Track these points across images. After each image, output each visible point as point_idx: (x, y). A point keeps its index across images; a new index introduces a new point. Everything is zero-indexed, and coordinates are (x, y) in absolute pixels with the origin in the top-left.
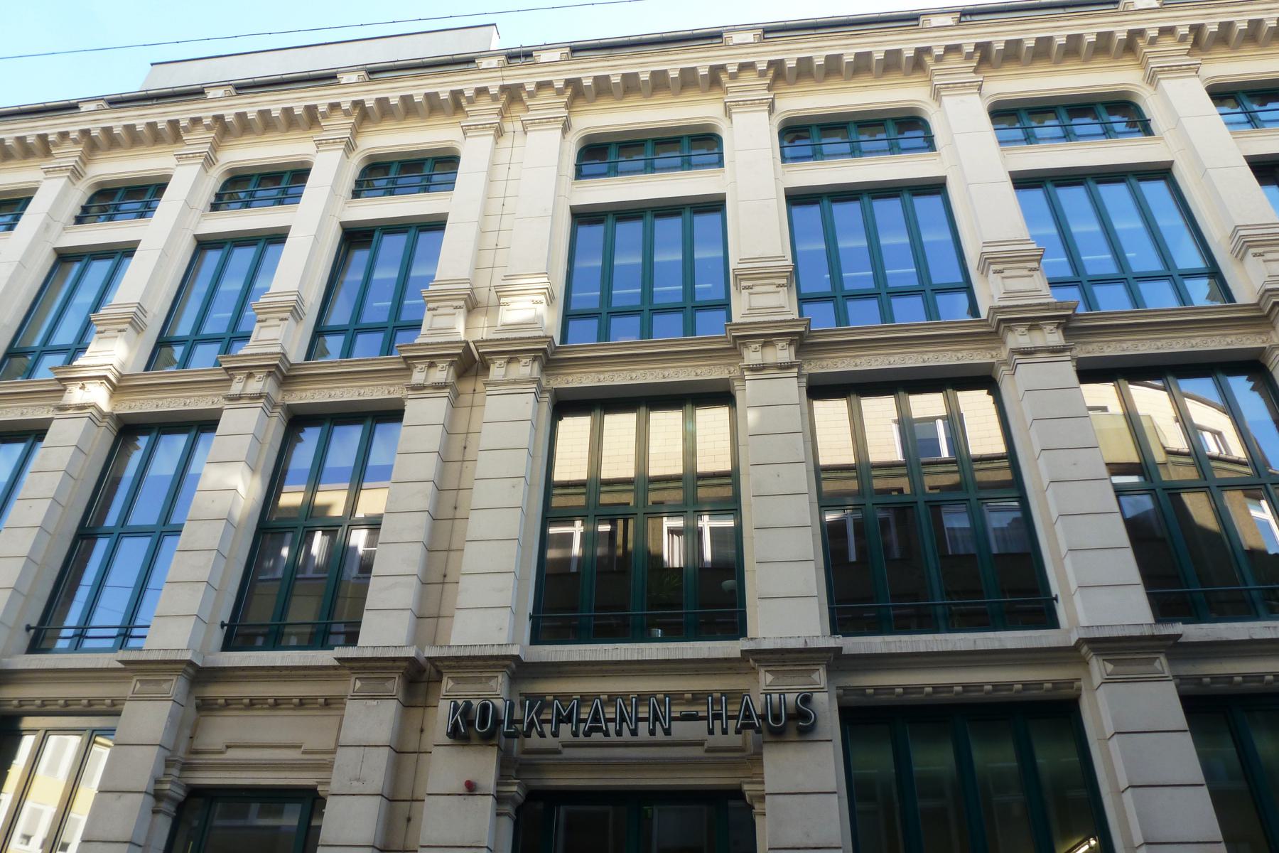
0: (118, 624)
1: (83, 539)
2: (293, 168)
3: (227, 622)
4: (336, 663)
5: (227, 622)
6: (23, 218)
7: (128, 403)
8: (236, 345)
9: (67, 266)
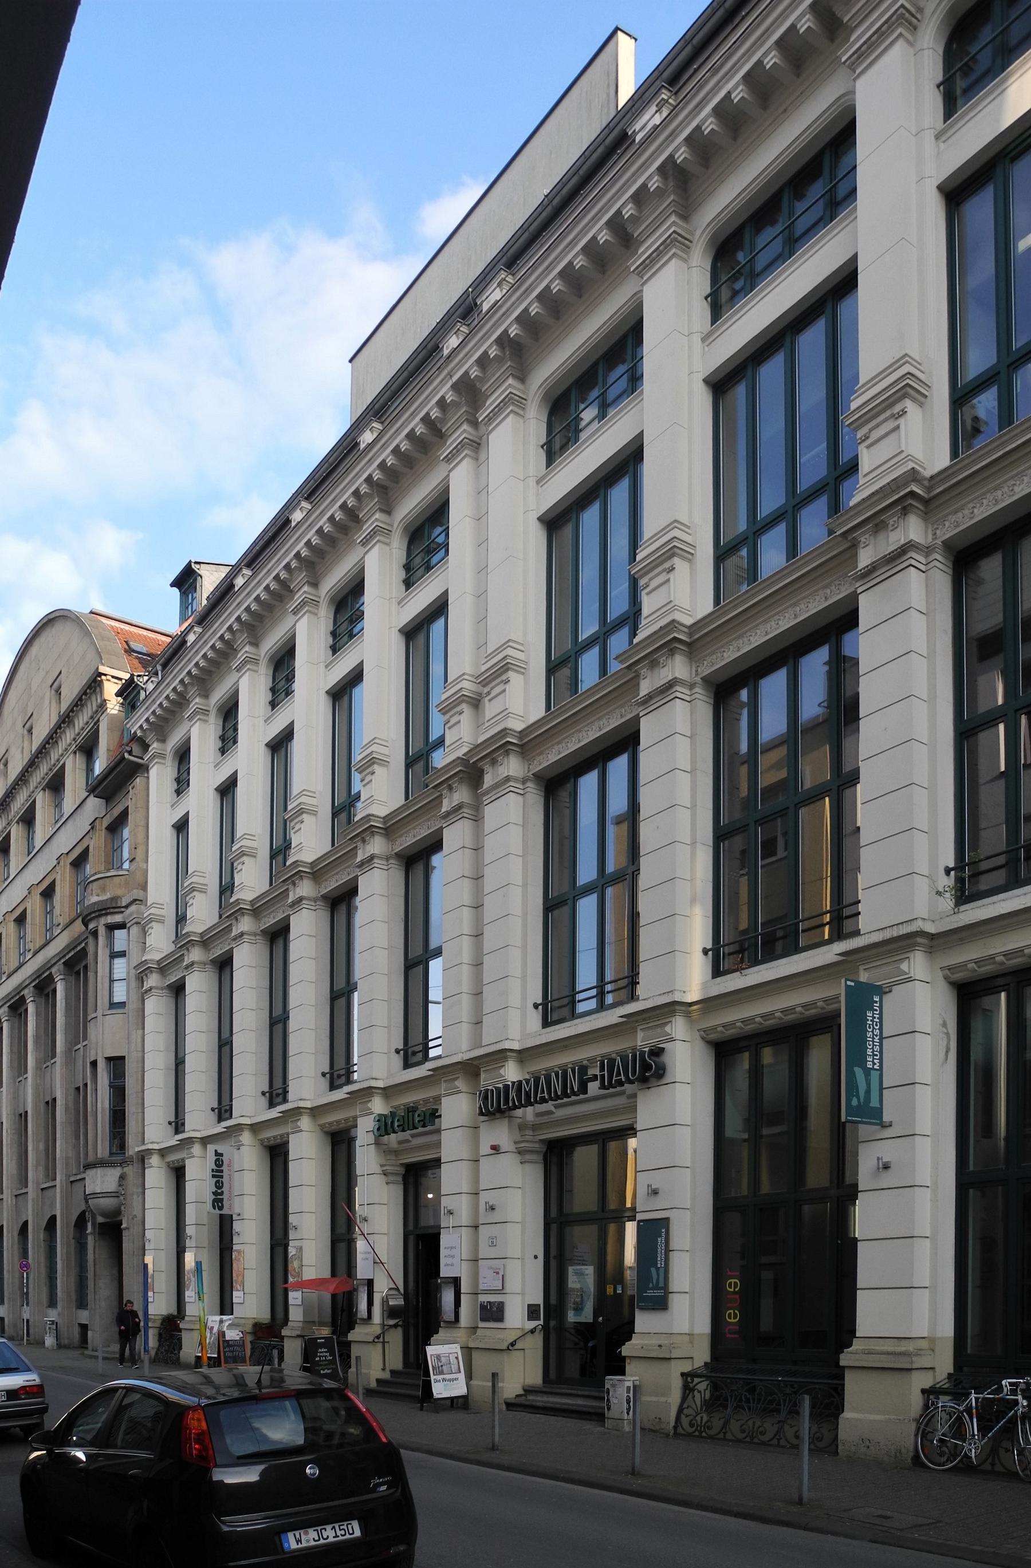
0: (1004, 848)
1: (723, 841)
2: (601, 352)
3: (952, 865)
4: (840, 958)
5: (952, 865)
6: (240, 727)
7: (952, 518)
8: (846, 485)
9: (730, 395)
